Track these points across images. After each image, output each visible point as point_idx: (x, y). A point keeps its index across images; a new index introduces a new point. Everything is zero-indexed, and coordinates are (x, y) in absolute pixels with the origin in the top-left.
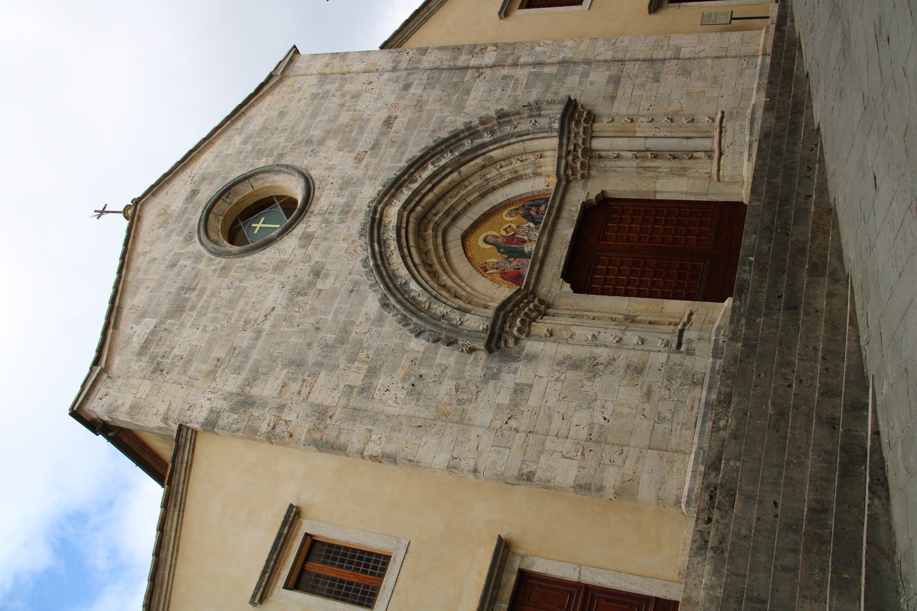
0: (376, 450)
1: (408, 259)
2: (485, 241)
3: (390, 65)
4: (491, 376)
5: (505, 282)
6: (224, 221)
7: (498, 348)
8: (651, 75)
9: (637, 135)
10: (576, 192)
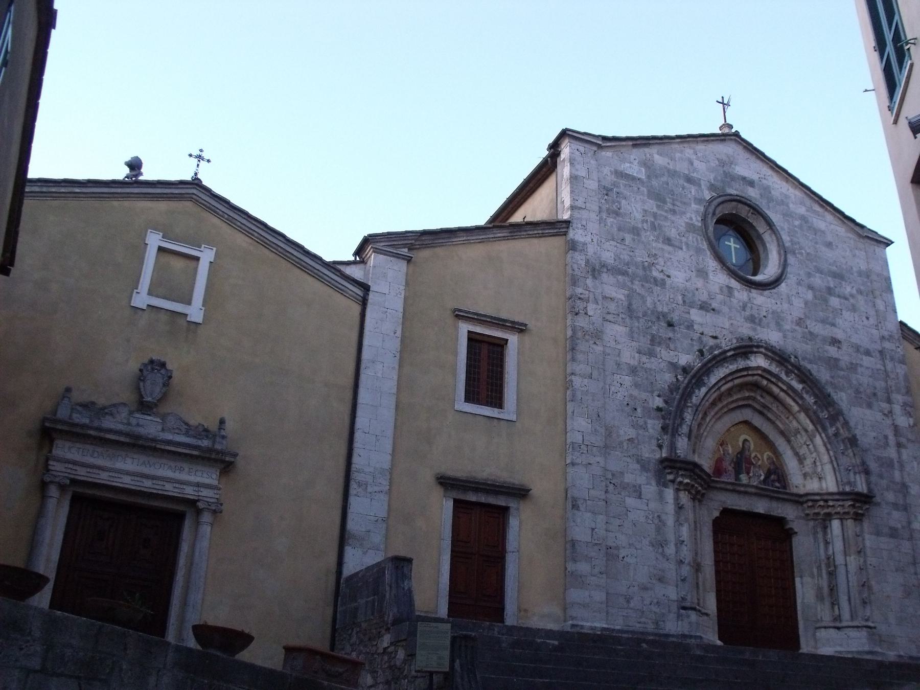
1: (724, 382)
2: (745, 440)
4: (644, 466)
5: (714, 463)
7: (665, 468)
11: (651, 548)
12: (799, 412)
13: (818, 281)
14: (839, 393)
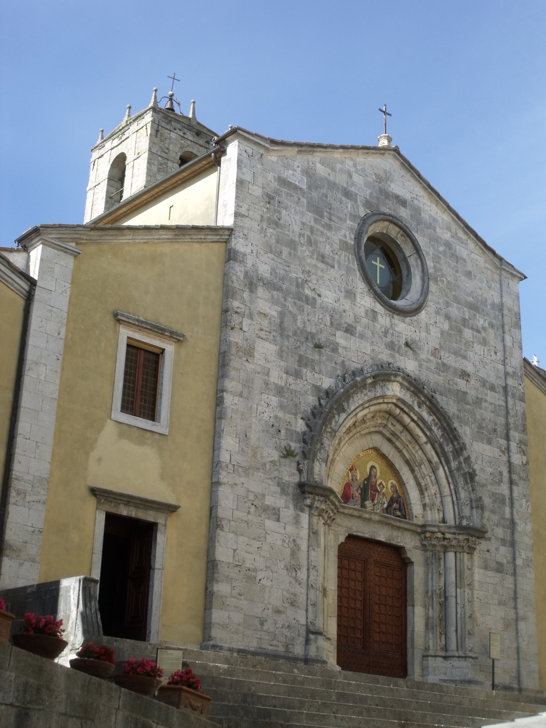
0: (228, 402)
2: (372, 467)
3: (510, 370)
4: (283, 487)
6: (383, 234)
8: (504, 598)
9: (458, 590)
10: (412, 541)
12: (426, 443)
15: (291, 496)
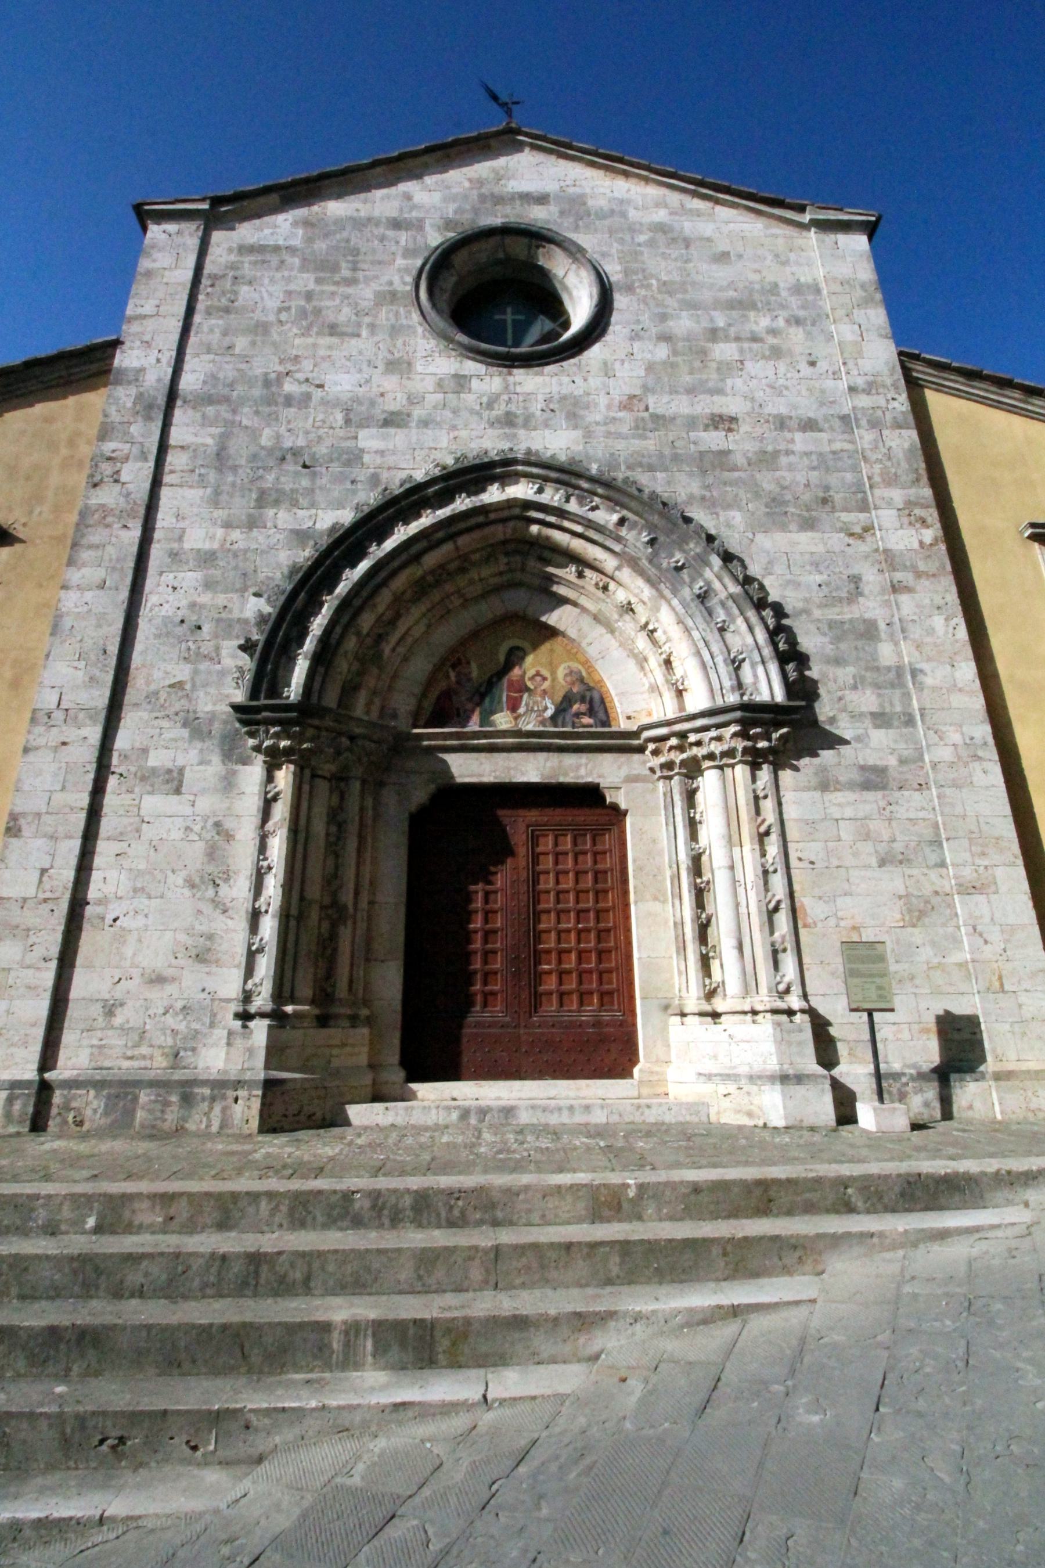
10: (619, 768)
11: (187, 892)
12: (618, 568)
13: (684, 324)
14: (721, 513)
15: (216, 742)
